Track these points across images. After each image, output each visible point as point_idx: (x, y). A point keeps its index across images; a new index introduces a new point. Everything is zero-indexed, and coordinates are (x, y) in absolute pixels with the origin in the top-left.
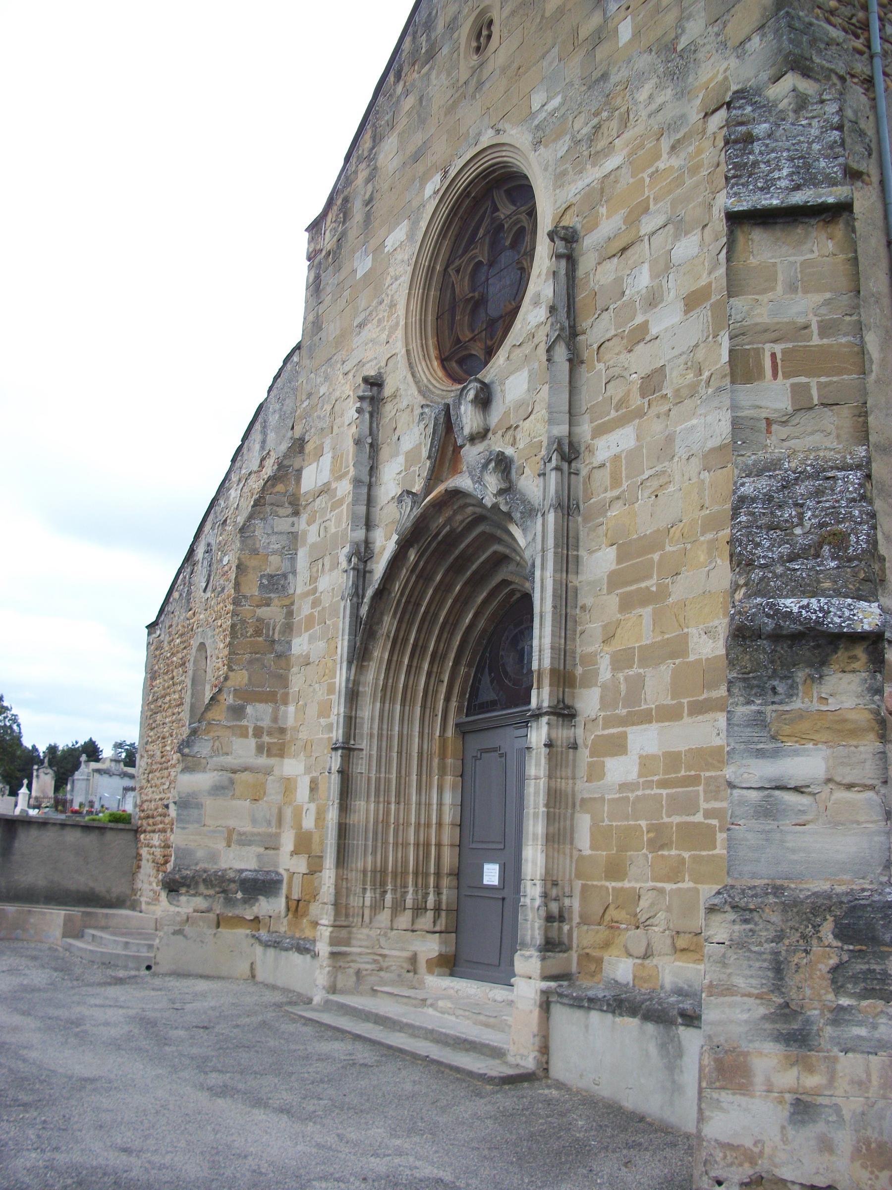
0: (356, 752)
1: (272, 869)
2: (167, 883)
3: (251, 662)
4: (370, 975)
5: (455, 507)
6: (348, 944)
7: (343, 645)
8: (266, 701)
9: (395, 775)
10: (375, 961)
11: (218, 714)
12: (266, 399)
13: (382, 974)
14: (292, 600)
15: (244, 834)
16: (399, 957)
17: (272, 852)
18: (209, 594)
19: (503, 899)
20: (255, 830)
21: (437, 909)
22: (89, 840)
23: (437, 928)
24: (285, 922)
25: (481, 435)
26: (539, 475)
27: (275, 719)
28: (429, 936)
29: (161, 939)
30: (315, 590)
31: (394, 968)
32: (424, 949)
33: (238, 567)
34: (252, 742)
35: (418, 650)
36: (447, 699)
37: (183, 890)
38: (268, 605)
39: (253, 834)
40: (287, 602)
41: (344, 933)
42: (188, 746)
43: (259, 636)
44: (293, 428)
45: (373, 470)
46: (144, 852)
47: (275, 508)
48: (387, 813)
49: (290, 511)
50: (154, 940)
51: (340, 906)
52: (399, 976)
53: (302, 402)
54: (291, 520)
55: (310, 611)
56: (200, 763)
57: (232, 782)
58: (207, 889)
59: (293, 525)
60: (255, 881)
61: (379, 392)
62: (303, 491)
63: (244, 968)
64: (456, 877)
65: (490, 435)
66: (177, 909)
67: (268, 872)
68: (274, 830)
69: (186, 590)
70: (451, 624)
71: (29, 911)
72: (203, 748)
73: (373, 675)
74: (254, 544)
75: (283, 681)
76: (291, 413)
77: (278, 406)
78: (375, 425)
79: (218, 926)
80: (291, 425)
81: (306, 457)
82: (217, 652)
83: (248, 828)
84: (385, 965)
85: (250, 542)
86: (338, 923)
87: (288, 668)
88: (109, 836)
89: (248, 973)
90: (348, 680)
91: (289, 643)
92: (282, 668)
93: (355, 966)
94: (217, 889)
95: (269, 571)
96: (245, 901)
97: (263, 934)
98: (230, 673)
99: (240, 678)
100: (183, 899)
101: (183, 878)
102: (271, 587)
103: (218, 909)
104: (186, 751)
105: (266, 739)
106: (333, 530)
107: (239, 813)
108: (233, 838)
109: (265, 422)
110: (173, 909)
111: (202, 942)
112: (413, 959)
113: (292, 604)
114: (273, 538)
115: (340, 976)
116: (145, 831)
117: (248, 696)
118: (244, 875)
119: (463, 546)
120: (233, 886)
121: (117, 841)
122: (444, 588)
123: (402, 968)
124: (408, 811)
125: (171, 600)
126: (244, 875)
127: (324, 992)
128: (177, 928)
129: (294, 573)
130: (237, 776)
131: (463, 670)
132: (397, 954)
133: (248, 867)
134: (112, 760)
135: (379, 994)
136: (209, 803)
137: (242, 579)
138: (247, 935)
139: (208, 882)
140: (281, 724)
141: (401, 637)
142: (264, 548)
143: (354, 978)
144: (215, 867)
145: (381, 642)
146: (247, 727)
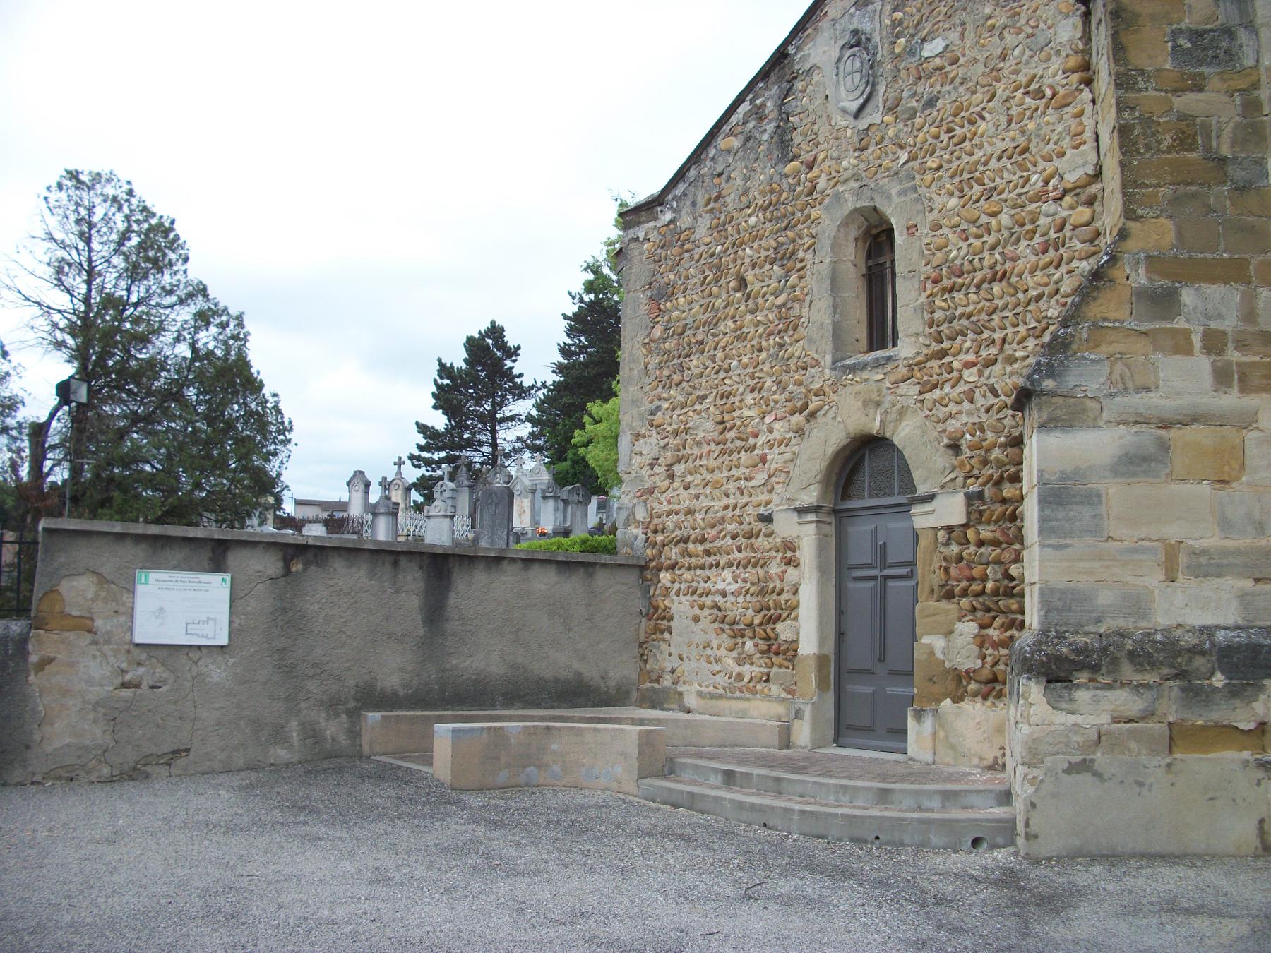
3: (1176, 201)
8: (1225, 280)
11: (1108, 307)
15: (1205, 552)
18: (874, 116)
20: (1229, 544)
22: (571, 586)
34: (1203, 364)
37: (1082, 678)
38: (1200, 89)
39: (1225, 553)
40: (1243, 83)
42: (1052, 374)
43: (1190, 150)
46: (680, 607)
56: (1084, 410)
57: (1164, 447)
66: (1072, 719)
69: (770, 127)
71: (548, 728)
83: (1212, 540)
88: (602, 577)
92: (1251, 213)
94: (1165, 671)
95: (1186, 23)
96: (1233, 692)
100: (1082, 695)
101: (1078, 651)
105: (1234, 356)
110: (1061, 718)
111: (1140, 784)
113: (1256, 86)
116: (672, 567)
120: (1199, 662)
121: (615, 589)
125: (712, 152)
128: (1077, 759)
129: (1250, 26)
130: (1173, 434)
133: (1221, 621)
136: (1113, 490)
137: (1126, 39)
138: (1246, 763)
139: (1140, 658)
144: (1143, 624)
146: (1187, 334)
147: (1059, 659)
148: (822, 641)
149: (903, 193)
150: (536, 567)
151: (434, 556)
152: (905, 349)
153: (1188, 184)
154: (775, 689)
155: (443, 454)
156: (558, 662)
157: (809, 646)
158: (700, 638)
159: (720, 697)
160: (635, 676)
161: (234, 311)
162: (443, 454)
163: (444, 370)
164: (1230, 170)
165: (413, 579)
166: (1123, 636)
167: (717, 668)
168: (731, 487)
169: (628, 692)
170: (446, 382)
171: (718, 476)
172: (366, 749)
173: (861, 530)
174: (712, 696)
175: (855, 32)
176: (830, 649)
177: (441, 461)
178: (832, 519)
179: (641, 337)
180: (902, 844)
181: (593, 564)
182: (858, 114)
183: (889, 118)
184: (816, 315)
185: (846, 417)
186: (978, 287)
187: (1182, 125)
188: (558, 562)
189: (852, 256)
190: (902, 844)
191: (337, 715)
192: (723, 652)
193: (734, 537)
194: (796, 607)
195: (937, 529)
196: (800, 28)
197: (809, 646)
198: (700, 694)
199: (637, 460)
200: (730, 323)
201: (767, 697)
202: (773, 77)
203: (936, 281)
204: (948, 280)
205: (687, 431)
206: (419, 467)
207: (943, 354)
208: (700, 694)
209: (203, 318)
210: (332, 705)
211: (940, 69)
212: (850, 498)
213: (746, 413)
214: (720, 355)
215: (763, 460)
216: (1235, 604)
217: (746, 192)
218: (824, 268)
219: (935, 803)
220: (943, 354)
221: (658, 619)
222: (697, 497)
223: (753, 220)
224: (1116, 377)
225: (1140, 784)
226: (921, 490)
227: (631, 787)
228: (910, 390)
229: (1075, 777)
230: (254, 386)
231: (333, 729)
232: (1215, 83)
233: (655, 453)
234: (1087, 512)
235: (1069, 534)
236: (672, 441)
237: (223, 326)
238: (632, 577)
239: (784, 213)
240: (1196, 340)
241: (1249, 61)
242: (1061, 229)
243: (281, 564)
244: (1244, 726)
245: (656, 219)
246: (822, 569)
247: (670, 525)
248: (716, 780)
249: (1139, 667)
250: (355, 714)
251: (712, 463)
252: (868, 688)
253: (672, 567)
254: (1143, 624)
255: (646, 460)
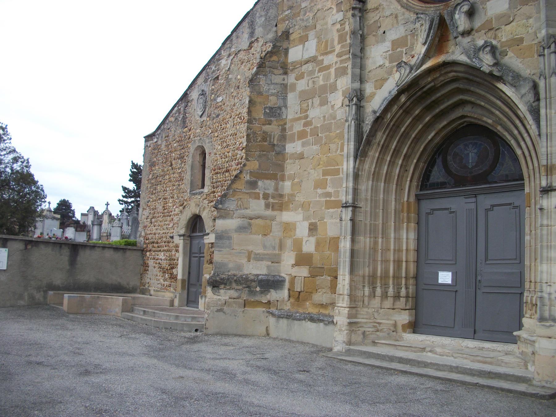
0: (358, 209)
1: (276, 274)
2: (212, 282)
3: (260, 156)
4: (371, 334)
5: (443, 72)
6: (356, 318)
7: (351, 147)
8: (271, 179)
9: (381, 222)
10: (375, 326)
11: (240, 185)
12: (252, 9)
13: (378, 333)
14: (284, 122)
15: (258, 254)
16: (388, 324)
17: (276, 264)
18: (204, 118)
19: (456, 291)
20: (265, 252)
21: (407, 297)
22: (118, 256)
23: (408, 307)
24: (289, 304)
25: (468, 33)
26: (540, 56)
27: (276, 189)
28: (403, 311)
29: (209, 314)
30: (307, 117)
31: (385, 330)
32: (400, 319)
33: (250, 102)
34: (262, 202)
35: (396, 152)
36: (411, 181)
37: (222, 286)
38: (270, 124)
39: (264, 254)
40: (282, 123)
41: (354, 311)
42: (221, 204)
43: (265, 142)
44: (276, 26)
45: (362, 50)
46: (151, 263)
47: (272, 69)
48: (376, 243)
49: (281, 71)
50: (204, 314)
51: (352, 297)
52: (388, 334)
53: (283, 11)
54: (283, 77)
55: (302, 128)
56: (229, 214)
57: (250, 225)
58: (237, 285)
59: (284, 80)
60: (268, 281)
61: (363, 6)
62: (289, 61)
63: (263, 330)
64: (415, 279)
65: (474, 32)
66: (219, 297)
67: (274, 276)
68: (277, 252)
69: (181, 116)
70: (417, 140)
71: (98, 297)
72: (231, 205)
73: (369, 165)
74: (260, 89)
75: (281, 168)
76: (275, 17)
77: (263, 13)
78: (362, 25)
79: (245, 307)
80: (275, 24)
81: (291, 42)
82: (215, 151)
83: (261, 251)
84: (380, 328)
85: (257, 88)
86: (352, 306)
87: (284, 160)
88: (128, 253)
89: (265, 333)
90: (354, 167)
91: (284, 146)
92: (280, 160)
93: (362, 329)
94: (244, 286)
95: (269, 105)
96: (262, 292)
97: (273, 310)
98: (247, 163)
99: (254, 165)
100: (222, 291)
101: (221, 279)
102: (271, 114)
103: (245, 297)
104: (220, 206)
105: (271, 200)
106: (321, 83)
107: (255, 242)
108: (250, 256)
109: (252, 22)
110: (215, 297)
111: (235, 316)
112: (395, 325)
113: (285, 124)
114: (272, 87)
115: (353, 335)
116: (150, 251)
117: (258, 176)
118: (260, 277)
119: (439, 95)
120: (253, 284)
121: (132, 256)
122: (418, 118)
123: (390, 330)
124: (388, 242)
125: (167, 121)
126: (260, 277)
127: (344, 345)
128: (219, 308)
129: (286, 107)
130: (253, 221)
131: (421, 165)
132: (386, 323)
133: (262, 273)
134: (47, 211)
135: (378, 345)
136: (235, 236)
137: (252, 109)
138: (264, 312)
139: (238, 282)
140: (280, 192)
141: (385, 145)
142: (266, 92)
143: (362, 336)
144: (241, 273)
145: (375, 147)
146: (259, 194)
147: (216, 281)
148: (183, 275)
149: (209, 143)
150: (107, 249)
151: (73, 245)
152: (206, 190)
153: (263, 151)
154: (172, 289)
155: (133, 199)
156: (113, 279)
157: (180, 277)
158: (155, 273)
159: (159, 291)
160: (139, 284)
161: (26, 158)
162: (133, 199)
163: (134, 166)
164: (276, 148)
165: (66, 252)
166: (234, 276)
167: (159, 282)
168: (165, 227)
169: (136, 290)
170: (135, 170)
171: (163, 223)
172: (48, 303)
173: (195, 242)
174: (157, 291)
175: (203, 91)
176: (186, 277)
177: (132, 202)
178: (189, 239)
179: (146, 178)
180: (177, 330)
181: (126, 249)
182: (201, 116)
183: (208, 119)
184: (187, 177)
185: (192, 210)
186: (223, 173)
187: (264, 135)
188: (114, 248)
189: (198, 158)
190: (177, 330)
191: (40, 292)
192: (160, 278)
193: (165, 242)
194: (178, 265)
195: (209, 243)
196: (191, 86)
197: (180, 277)
198: (154, 290)
199: (143, 217)
200: (168, 176)
201: (170, 292)
202: (183, 101)
203: (214, 170)
204: (217, 171)
205: (155, 209)
206: (122, 204)
207: (214, 192)
208: (154, 290)
209: (16, 160)
210: (39, 289)
211: (221, 106)
212: (196, 232)
213: (170, 205)
214: (165, 186)
215: (172, 219)
216: (266, 268)
217: (174, 135)
218: (190, 162)
219: (190, 320)
220: (214, 192)
221: (145, 266)
222: (157, 229)
223: (175, 145)
224: (239, 205)
225: (235, 316)
226: (207, 231)
227: (120, 315)
228: (206, 202)
229: (218, 313)
230: (35, 183)
231: (39, 296)
232: (275, 122)
233: (148, 215)
234: (228, 242)
235: (222, 247)
236: (152, 212)
237: (23, 162)
238: (139, 253)
239: (183, 142)
240: (261, 196)
241: (284, 117)
242: (241, 159)
243: (24, 246)
244: (264, 302)
245: (152, 140)
246: (184, 253)
247: (150, 238)
248: (142, 313)
249: (237, 285)
250: (45, 292)
251: (161, 219)
252: (191, 290)
253: (150, 251)
254: (241, 273)
255: (145, 217)
